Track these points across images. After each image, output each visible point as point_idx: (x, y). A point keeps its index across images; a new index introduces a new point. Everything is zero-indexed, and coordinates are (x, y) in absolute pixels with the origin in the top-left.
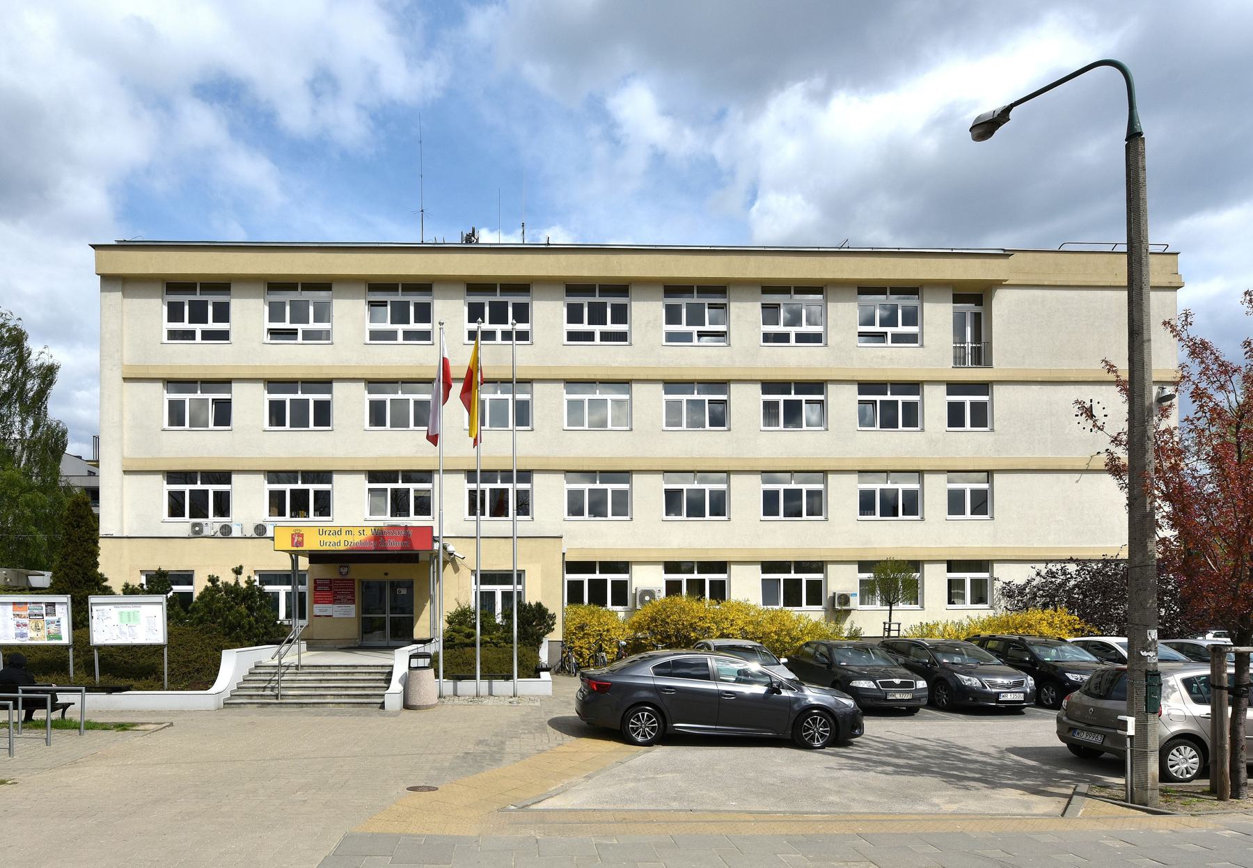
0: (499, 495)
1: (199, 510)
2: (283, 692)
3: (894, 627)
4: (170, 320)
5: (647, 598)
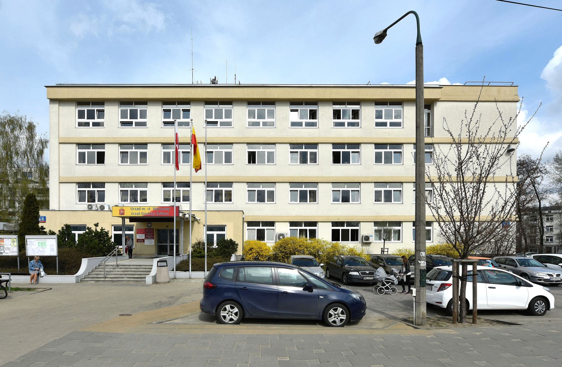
0: (220, 192)
1: (92, 198)
2: (108, 276)
3: (386, 250)
4: (249, 118)
5: (281, 237)
